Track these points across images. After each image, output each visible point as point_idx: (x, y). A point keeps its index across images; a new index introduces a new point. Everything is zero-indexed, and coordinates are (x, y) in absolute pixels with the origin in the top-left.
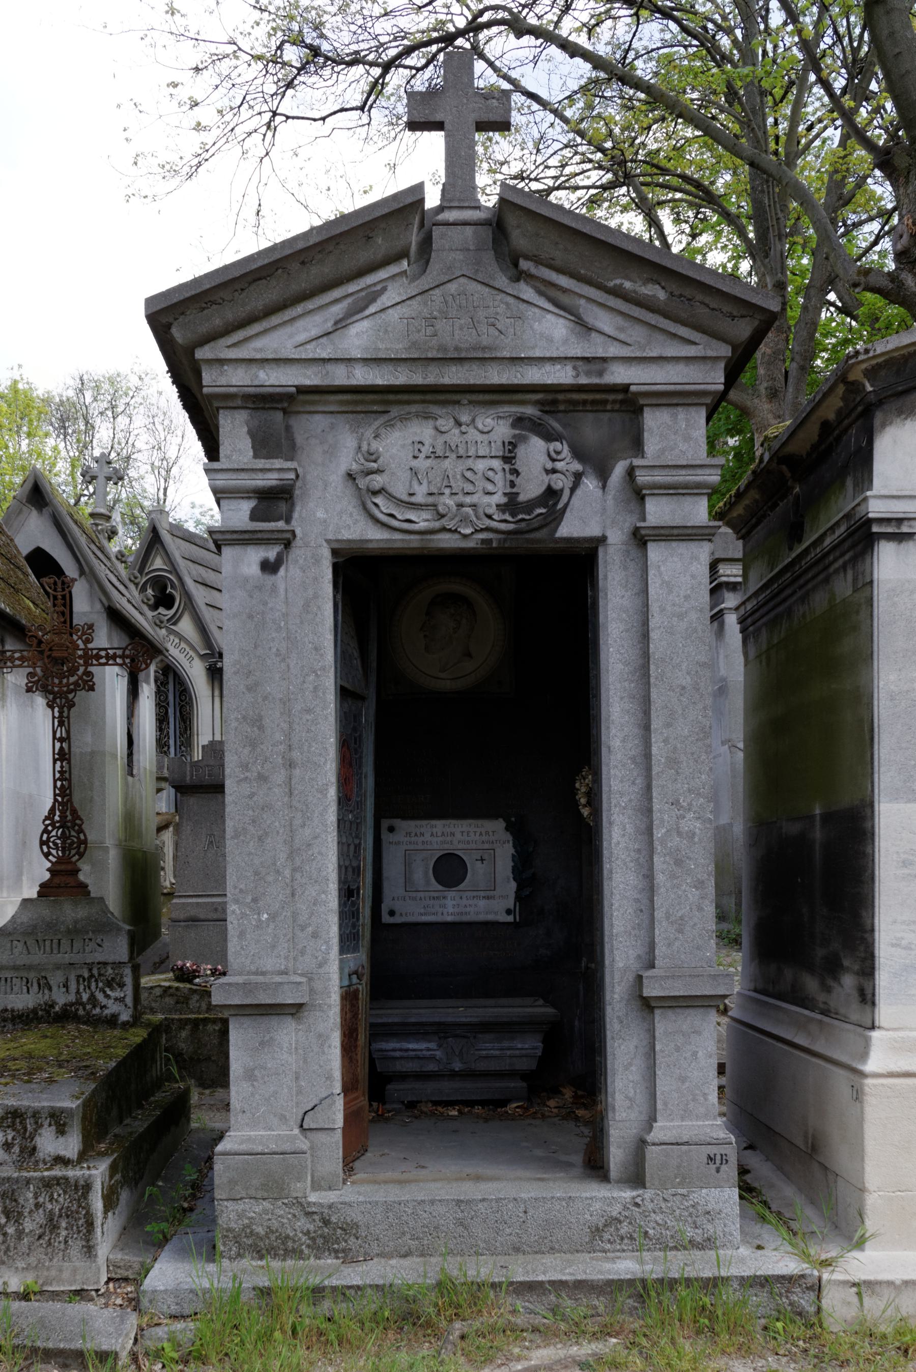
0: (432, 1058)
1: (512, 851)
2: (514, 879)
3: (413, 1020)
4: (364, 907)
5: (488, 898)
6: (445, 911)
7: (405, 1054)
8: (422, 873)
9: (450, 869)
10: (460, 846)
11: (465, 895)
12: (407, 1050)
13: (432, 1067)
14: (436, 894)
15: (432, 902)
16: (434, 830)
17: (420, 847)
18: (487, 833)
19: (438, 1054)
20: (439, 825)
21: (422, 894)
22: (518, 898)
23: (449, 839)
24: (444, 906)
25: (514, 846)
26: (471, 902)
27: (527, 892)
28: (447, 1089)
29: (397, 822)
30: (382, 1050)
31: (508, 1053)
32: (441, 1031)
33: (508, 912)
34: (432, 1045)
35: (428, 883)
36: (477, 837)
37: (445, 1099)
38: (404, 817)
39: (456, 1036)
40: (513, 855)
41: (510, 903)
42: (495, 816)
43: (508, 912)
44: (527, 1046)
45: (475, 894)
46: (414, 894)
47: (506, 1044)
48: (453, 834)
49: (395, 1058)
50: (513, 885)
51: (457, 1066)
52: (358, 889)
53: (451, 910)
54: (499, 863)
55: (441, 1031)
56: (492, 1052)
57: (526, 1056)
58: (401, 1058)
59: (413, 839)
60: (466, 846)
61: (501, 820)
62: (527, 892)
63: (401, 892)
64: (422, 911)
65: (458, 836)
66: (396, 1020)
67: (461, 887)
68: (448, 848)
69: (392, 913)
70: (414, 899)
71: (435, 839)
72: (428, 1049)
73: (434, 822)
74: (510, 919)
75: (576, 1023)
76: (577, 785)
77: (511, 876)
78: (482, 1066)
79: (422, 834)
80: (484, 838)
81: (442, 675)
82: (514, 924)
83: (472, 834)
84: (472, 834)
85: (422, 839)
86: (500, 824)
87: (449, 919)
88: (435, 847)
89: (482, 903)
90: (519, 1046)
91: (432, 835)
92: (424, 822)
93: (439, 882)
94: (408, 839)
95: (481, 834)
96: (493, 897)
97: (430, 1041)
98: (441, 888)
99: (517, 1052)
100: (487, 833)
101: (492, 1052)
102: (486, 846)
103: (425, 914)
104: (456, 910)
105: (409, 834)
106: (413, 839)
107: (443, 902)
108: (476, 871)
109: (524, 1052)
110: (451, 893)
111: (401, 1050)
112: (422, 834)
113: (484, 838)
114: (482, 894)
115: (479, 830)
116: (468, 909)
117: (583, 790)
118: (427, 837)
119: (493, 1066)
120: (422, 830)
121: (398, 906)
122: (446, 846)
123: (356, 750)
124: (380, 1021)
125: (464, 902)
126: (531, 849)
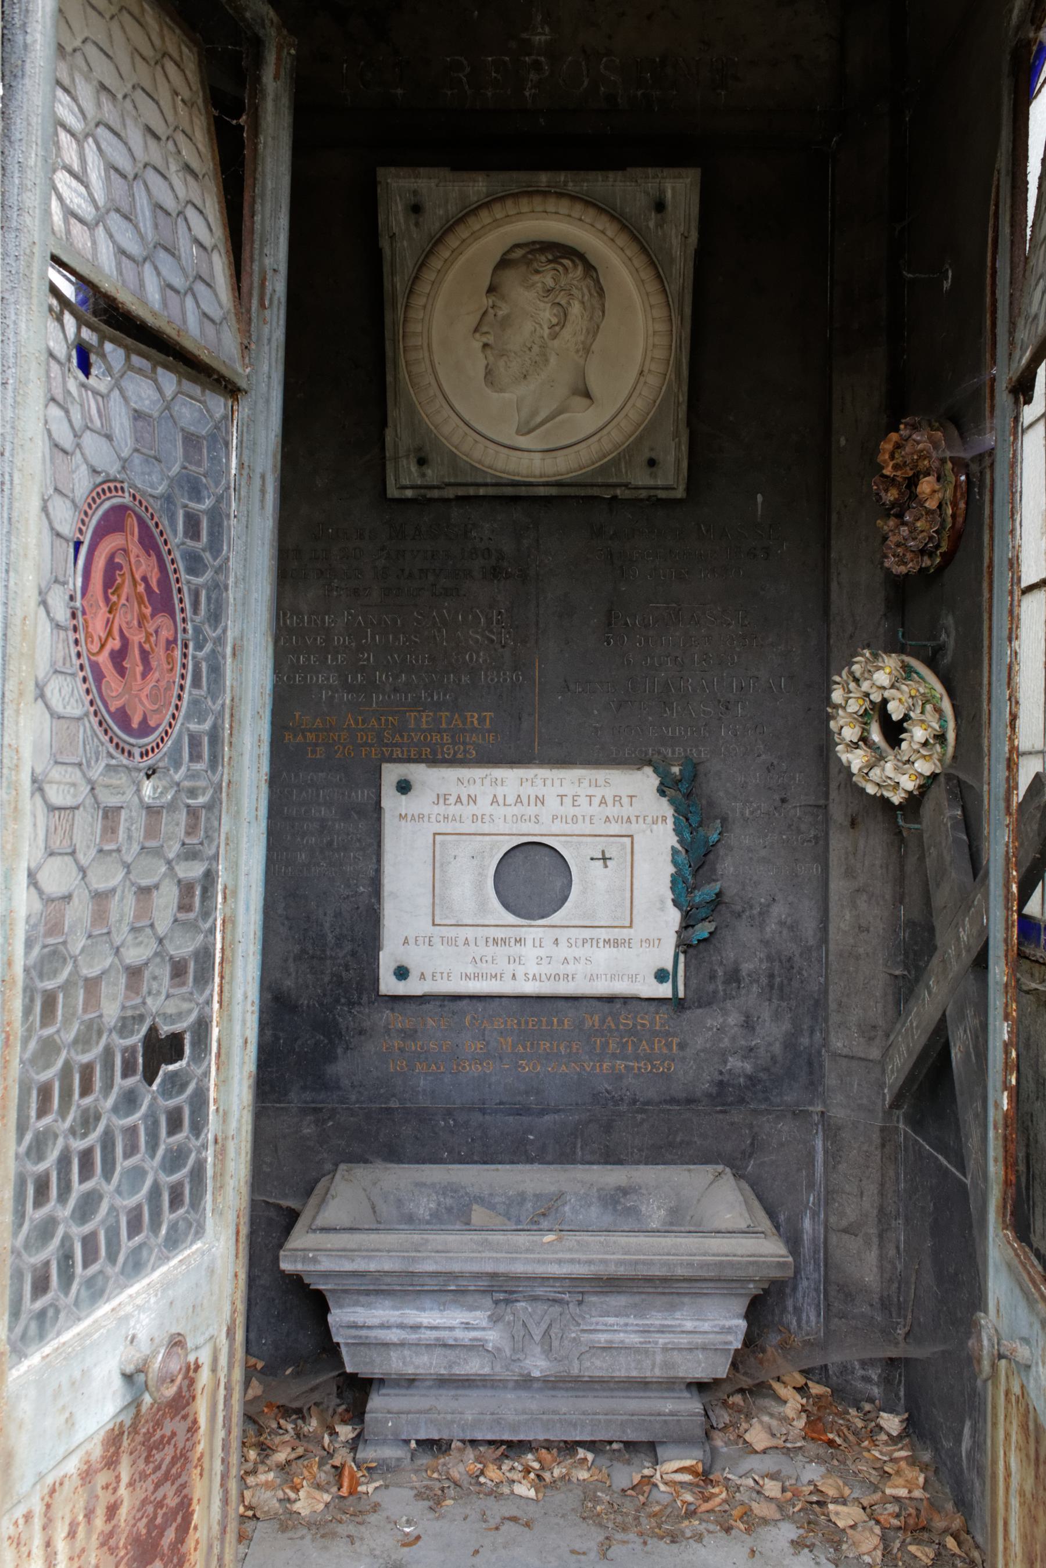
0: (476, 1347)
1: (673, 840)
2: (676, 903)
3: (429, 1267)
4: (223, 1082)
5: (616, 943)
6: (520, 971)
7: (413, 1337)
8: (472, 884)
9: (532, 879)
10: (557, 827)
11: (563, 935)
12: (416, 1328)
13: (474, 1366)
14: (500, 933)
15: (492, 949)
16: (500, 791)
17: (467, 827)
18: (617, 799)
19: (493, 1337)
20: (510, 780)
21: (469, 933)
22: (684, 946)
23: (532, 810)
24: (518, 960)
25: (677, 831)
26: (578, 952)
27: (703, 930)
28: (515, 1414)
29: (417, 772)
30: (355, 1326)
31: (662, 1340)
32: (501, 1290)
33: (661, 976)
34: (479, 1317)
35: (482, 906)
36: (595, 808)
37: (506, 1437)
38: (435, 760)
39: (535, 1299)
40: (674, 851)
41: (665, 955)
42: (639, 762)
43: (661, 976)
44: (706, 1326)
45: (587, 933)
46: (452, 932)
47: (656, 1319)
48: (541, 800)
49: (386, 1345)
50: (674, 917)
51: (538, 1365)
52: (202, 1027)
53: (533, 969)
54: (642, 867)
55: (501, 1290)
56: (624, 1337)
57: (704, 1349)
58: (402, 1344)
59: (453, 810)
60: (568, 829)
61: (648, 770)
62: (703, 930)
63: (423, 925)
64: (470, 969)
65: (552, 803)
66: (387, 1266)
67: (556, 918)
68: (531, 831)
69: (402, 973)
70: (452, 942)
71: (502, 810)
72: (467, 1327)
73: (499, 773)
74: (664, 990)
75: (807, 1224)
76: (837, 696)
77: (670, 896)
78: (597, 1367)
79: (473, 799)
80: (612, 810)
81: (522, 442)
82: (677, 1004)
83: (583, 801)
84: (583, 801)
85: (472, 809)
86: (647, 780)
87: (530, 988)
88: (503, 828)
89: (603, 956)
90: (689, 1325)
91: (495, 801)
92: (478, 773)
93: (507, 906)
94: (441, 809)
95: (603, 802)
96: (628, 943)
97: (471, 1308)
98: (511, 919)
99: (684, 1340)
100: (617, 799)
101: (624, 1337)
102: (614, 828)
103: (476, 977)
104: (546, 969)
105: (442, 798)
106: (453, 810)
107: (515, 950)
108: (591, 886)
109: (699, 1339)
110: (534, 932)
111: (401, 1326)
112: (473, 799)
113: (612, 810)
114: (603, 934)
115: (598, 793)
116: (570, 968)
117: (853, 706)
118: (484, 806)
119: (624, 1368)
120: (473, 790)
121: (414, 958)
122: (526, 827)
123: (195, 564)
124: (348, 1266)
125: (563, 951)
126: (715, 837)
